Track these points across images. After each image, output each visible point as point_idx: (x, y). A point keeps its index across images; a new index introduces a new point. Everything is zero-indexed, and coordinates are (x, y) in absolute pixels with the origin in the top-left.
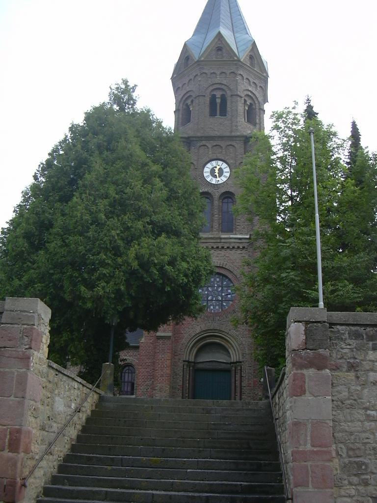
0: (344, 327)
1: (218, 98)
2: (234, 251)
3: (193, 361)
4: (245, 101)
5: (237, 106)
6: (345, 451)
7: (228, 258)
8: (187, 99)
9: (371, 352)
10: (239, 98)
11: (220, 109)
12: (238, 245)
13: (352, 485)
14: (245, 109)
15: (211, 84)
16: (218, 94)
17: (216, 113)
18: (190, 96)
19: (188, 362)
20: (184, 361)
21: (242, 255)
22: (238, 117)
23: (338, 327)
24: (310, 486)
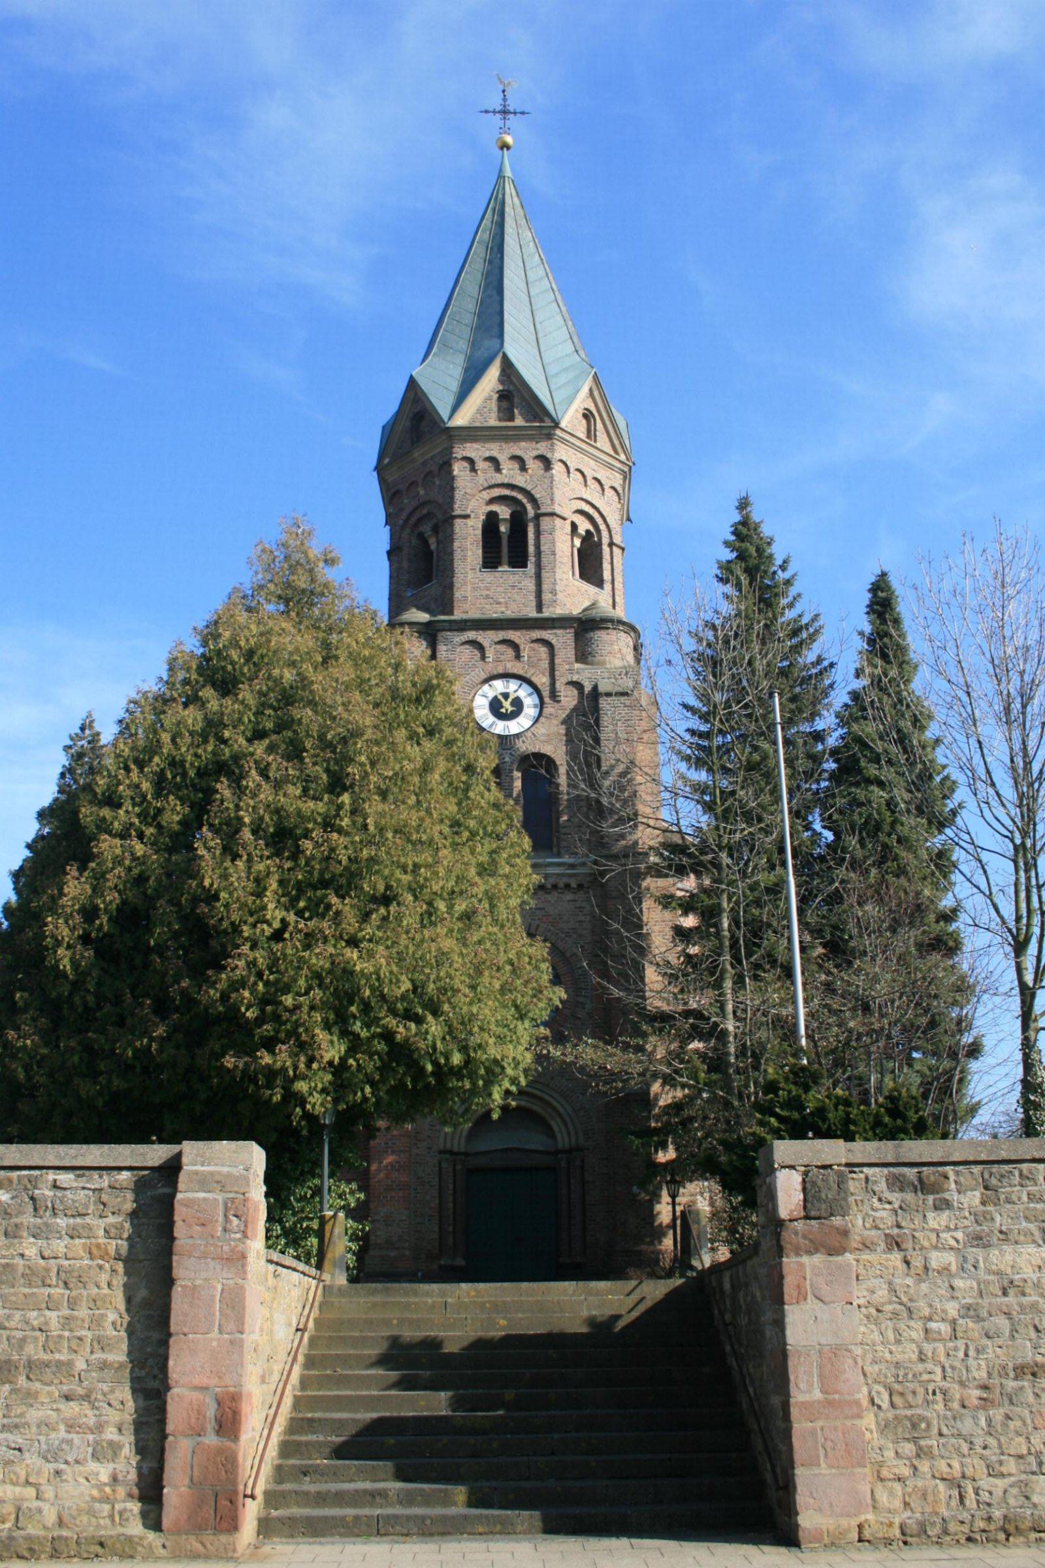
0: (877, 1170)
1: (505, 520)
2: (555, 894)
3: (463, 1149)
4: (574, 526)
5: (553, 543)
6: (886, 1396)
7: (543, 912)
8: (420, 521)
9: (930, 1215)
10: (558, 521)
11: (509, 547)
12: (565, 880)
13: (902, 1458)
14: (573, 546)
15: (486, 485)
16: (504, 512)
17: (500, 557)
18: (429, 515)
19: (451, 1153)
20: (441, 1152)
21: (578, 904)
22: (557, 570)
23: (865, 1169)
24: (823, 1465)
